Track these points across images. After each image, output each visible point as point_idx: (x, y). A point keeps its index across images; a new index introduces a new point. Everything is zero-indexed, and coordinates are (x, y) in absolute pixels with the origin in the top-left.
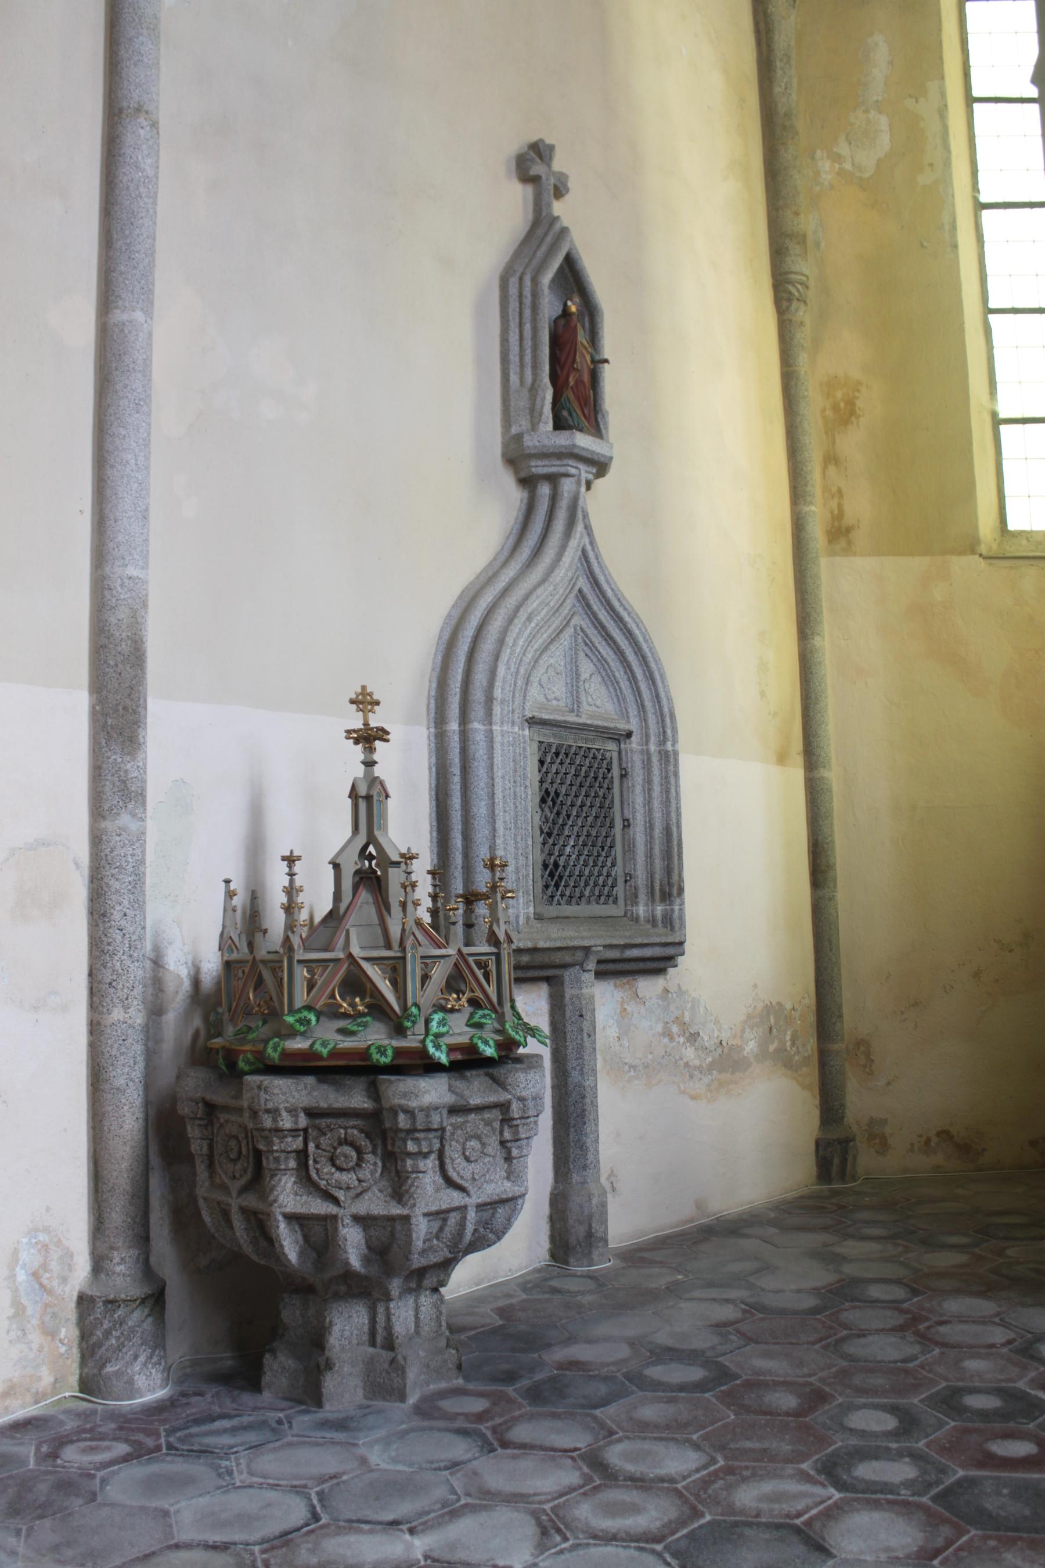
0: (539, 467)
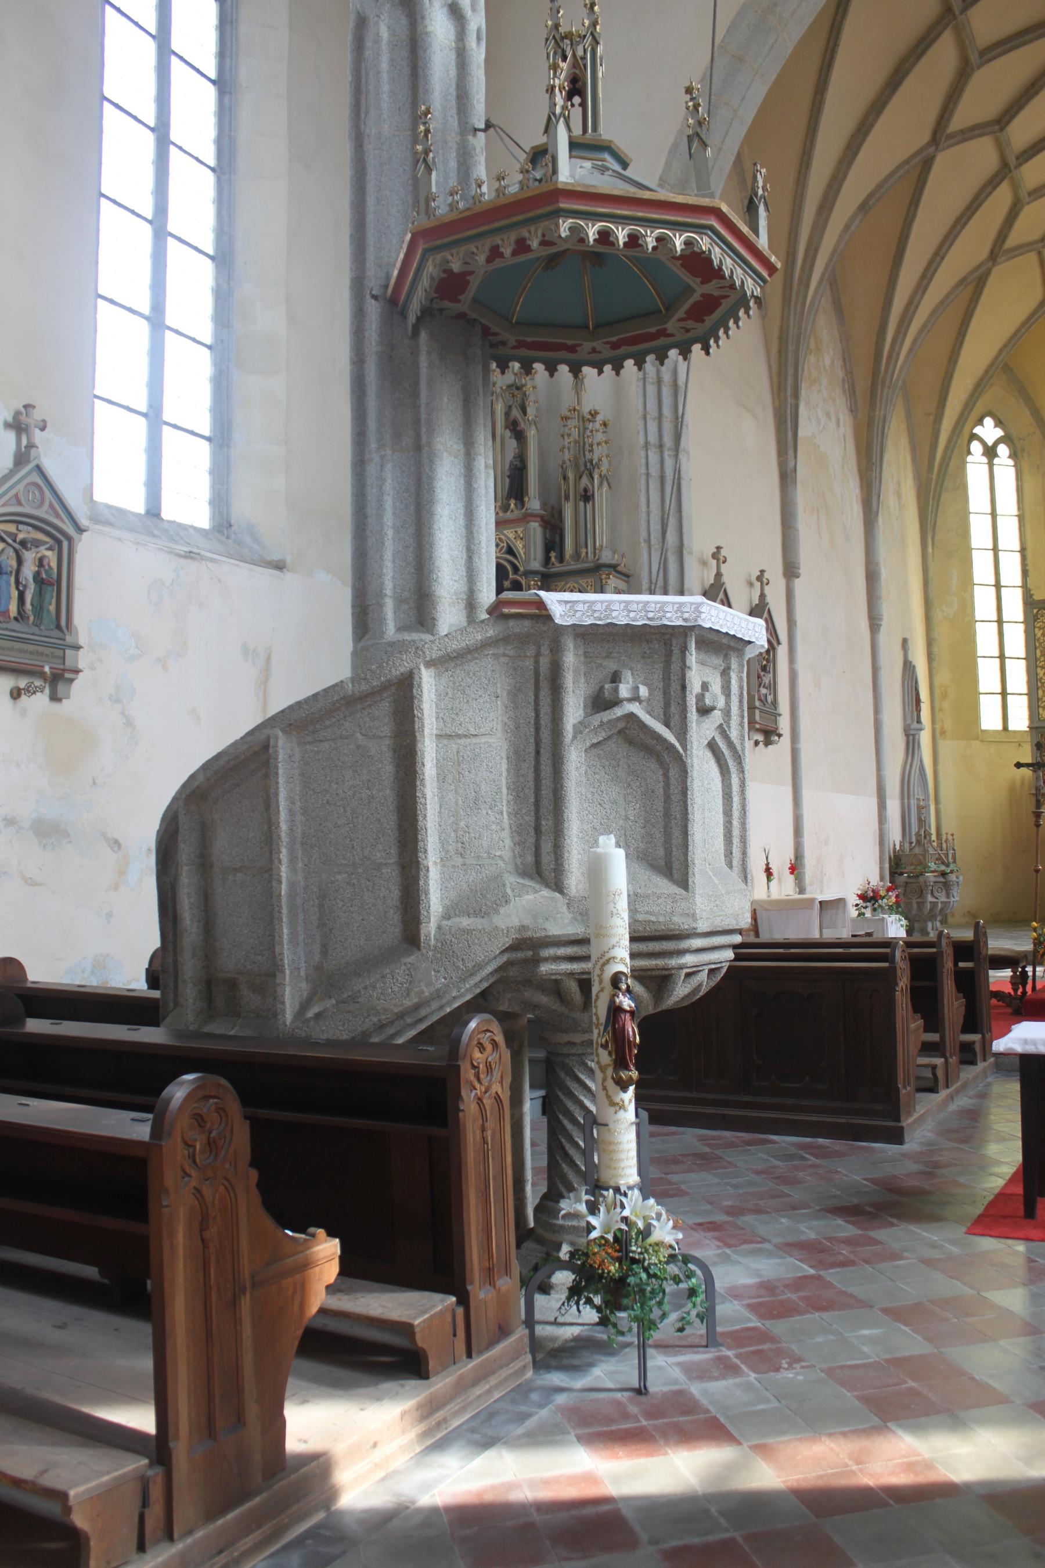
0: (912, 732)
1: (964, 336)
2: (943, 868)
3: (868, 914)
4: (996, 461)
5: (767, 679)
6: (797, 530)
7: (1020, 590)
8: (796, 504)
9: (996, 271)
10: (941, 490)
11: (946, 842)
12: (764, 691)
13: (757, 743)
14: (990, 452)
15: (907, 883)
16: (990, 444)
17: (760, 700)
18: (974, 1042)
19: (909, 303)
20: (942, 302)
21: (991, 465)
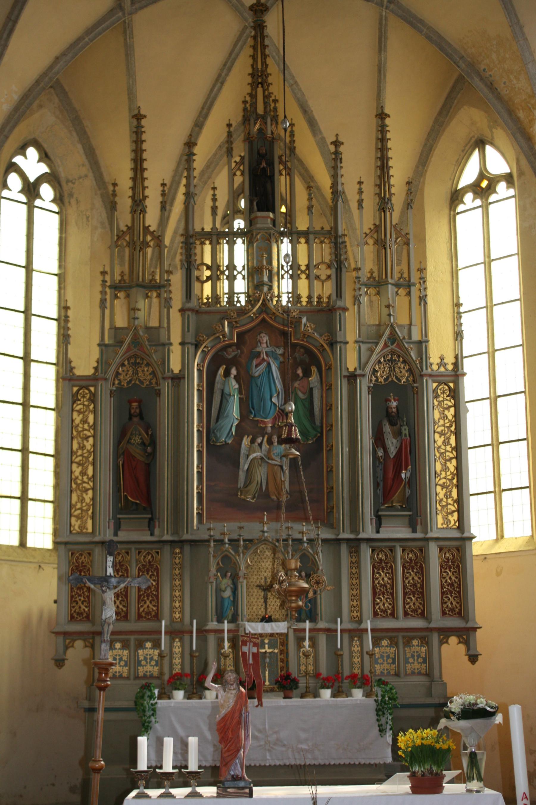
1: (15, 22)
4: (38, 202)
14: (31, 190)
16: (32, 179)
21: (31, 208)
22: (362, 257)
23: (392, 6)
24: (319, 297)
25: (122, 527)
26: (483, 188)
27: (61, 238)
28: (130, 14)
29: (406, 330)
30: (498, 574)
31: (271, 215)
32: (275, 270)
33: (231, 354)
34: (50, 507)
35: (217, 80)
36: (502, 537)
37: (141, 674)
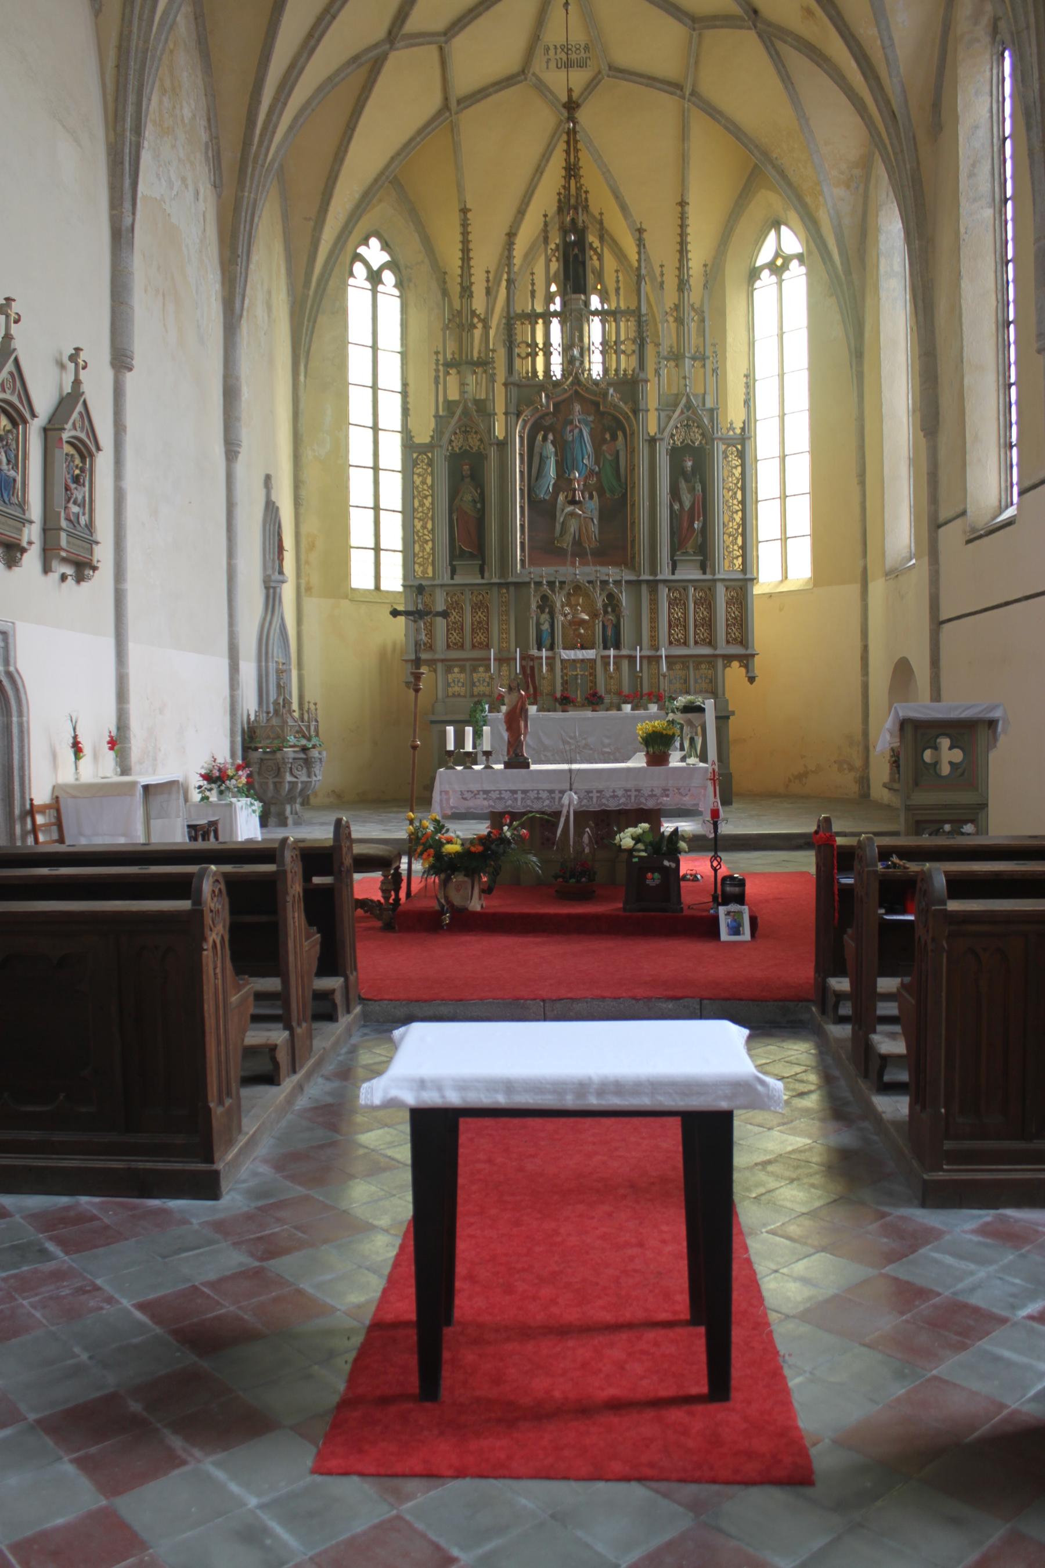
0: (273, 584)
1: (353, 130)
2: (304, 742)
3: (213, 797)
4: (380, 288)
5: (78, 494)
6: (132, 308)
7: (398, 436)
8: (132, 273)
9: (393, 56)
10: (318, 311)
11: (308, 712)
12: (75, 509)
13: (64, 578)
14: (374, 277)
15: (262, 760)
16: (375, 268)
17: (68, 519)
18: (333, 991)
19: (292, 66)
20: (330, 79)
21: (374, 292)
22: (667, 333)
23: (693, 99)
24: (625, 371)
25: (458, 571)
26: (777, 268)
27: (402, 320)
28: (457, 113)
29: (700, 399)
30: (781, 610)
31: (583, 297)
32: (586, 346)
33: (548, 422)
34: (400, 556)
35: (537, 170)
36: (786, 578)
37: (475, 693)
